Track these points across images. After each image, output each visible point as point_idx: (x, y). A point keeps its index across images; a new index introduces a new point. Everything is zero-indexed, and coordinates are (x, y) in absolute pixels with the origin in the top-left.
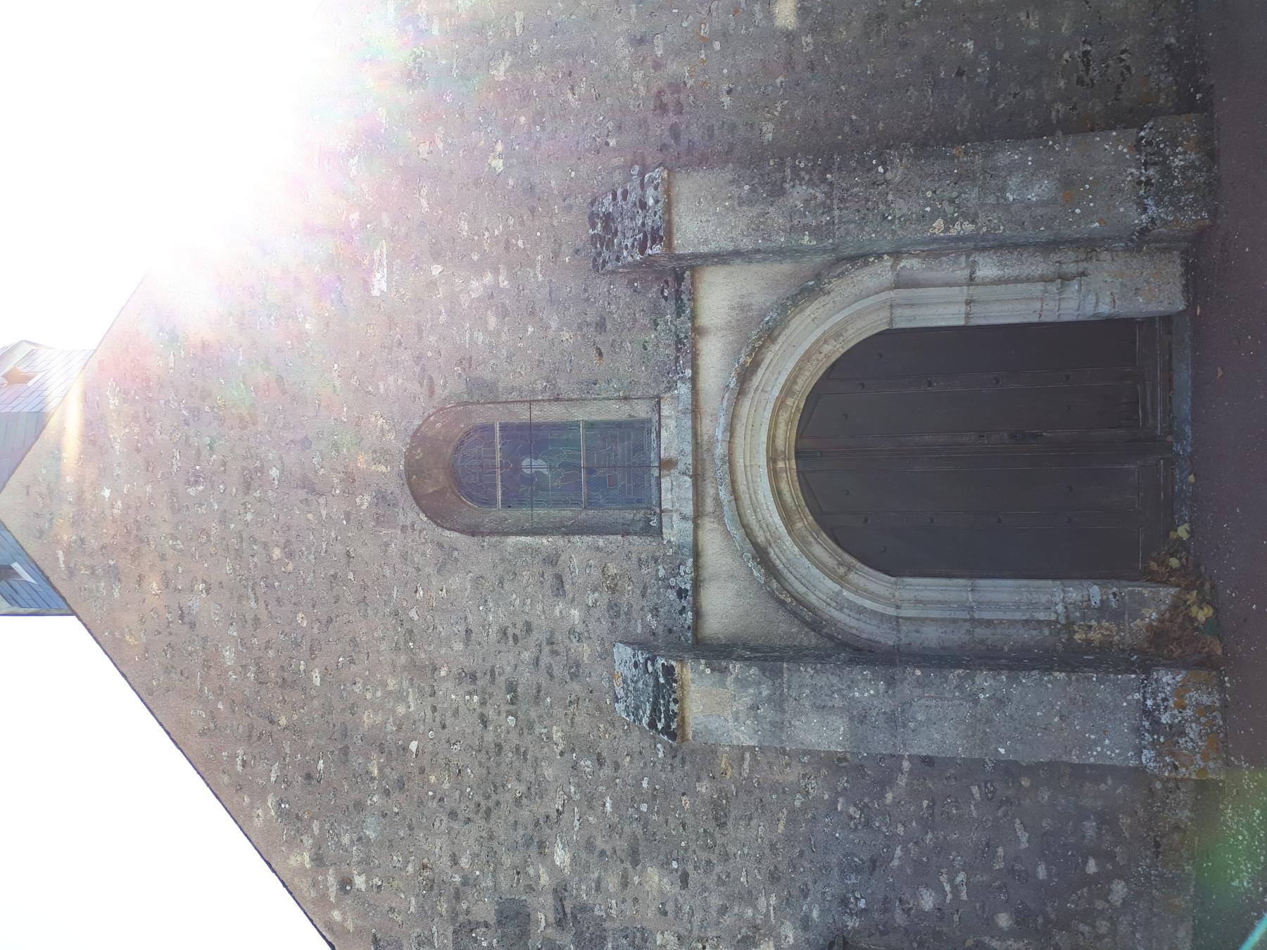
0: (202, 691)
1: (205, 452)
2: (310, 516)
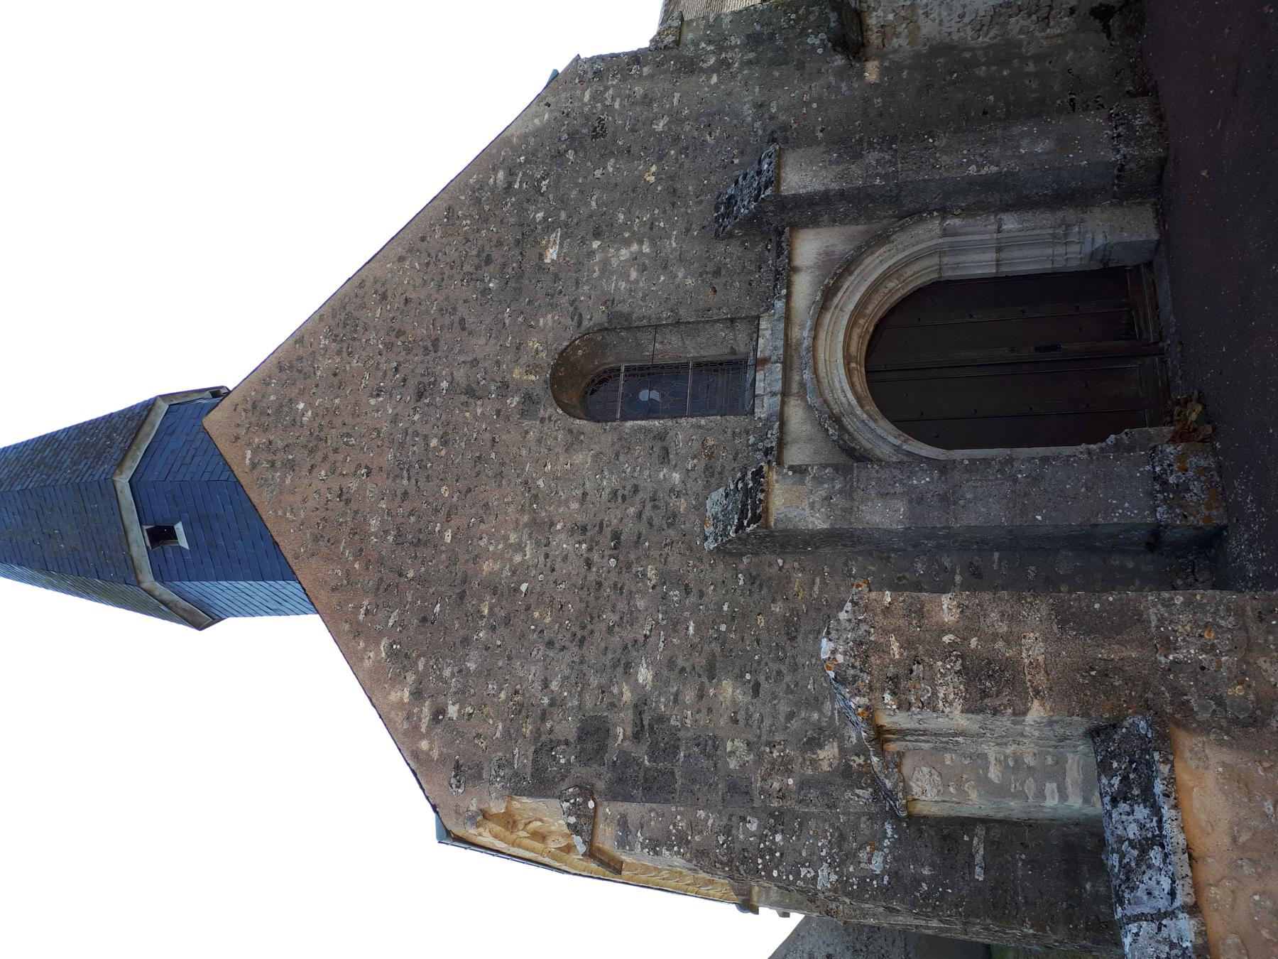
0: (343, 553)
1: (390, 374)
2: (467, 414)
